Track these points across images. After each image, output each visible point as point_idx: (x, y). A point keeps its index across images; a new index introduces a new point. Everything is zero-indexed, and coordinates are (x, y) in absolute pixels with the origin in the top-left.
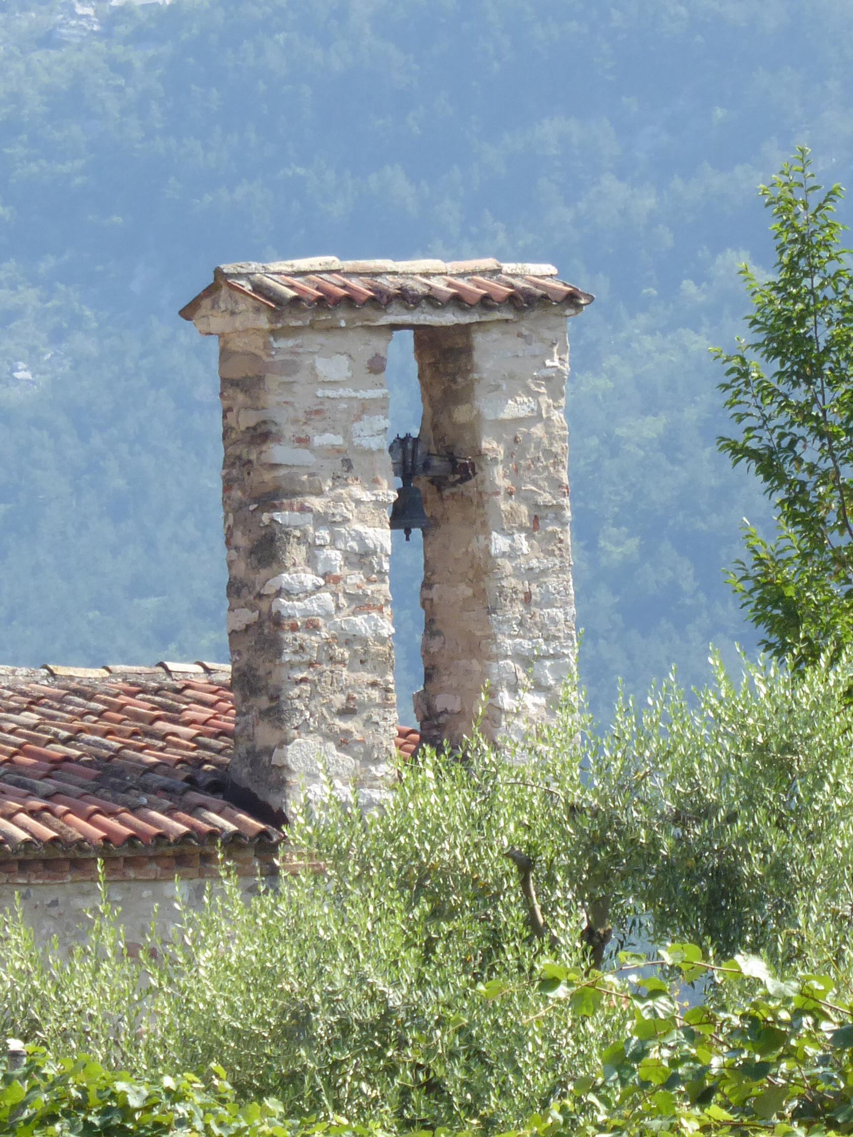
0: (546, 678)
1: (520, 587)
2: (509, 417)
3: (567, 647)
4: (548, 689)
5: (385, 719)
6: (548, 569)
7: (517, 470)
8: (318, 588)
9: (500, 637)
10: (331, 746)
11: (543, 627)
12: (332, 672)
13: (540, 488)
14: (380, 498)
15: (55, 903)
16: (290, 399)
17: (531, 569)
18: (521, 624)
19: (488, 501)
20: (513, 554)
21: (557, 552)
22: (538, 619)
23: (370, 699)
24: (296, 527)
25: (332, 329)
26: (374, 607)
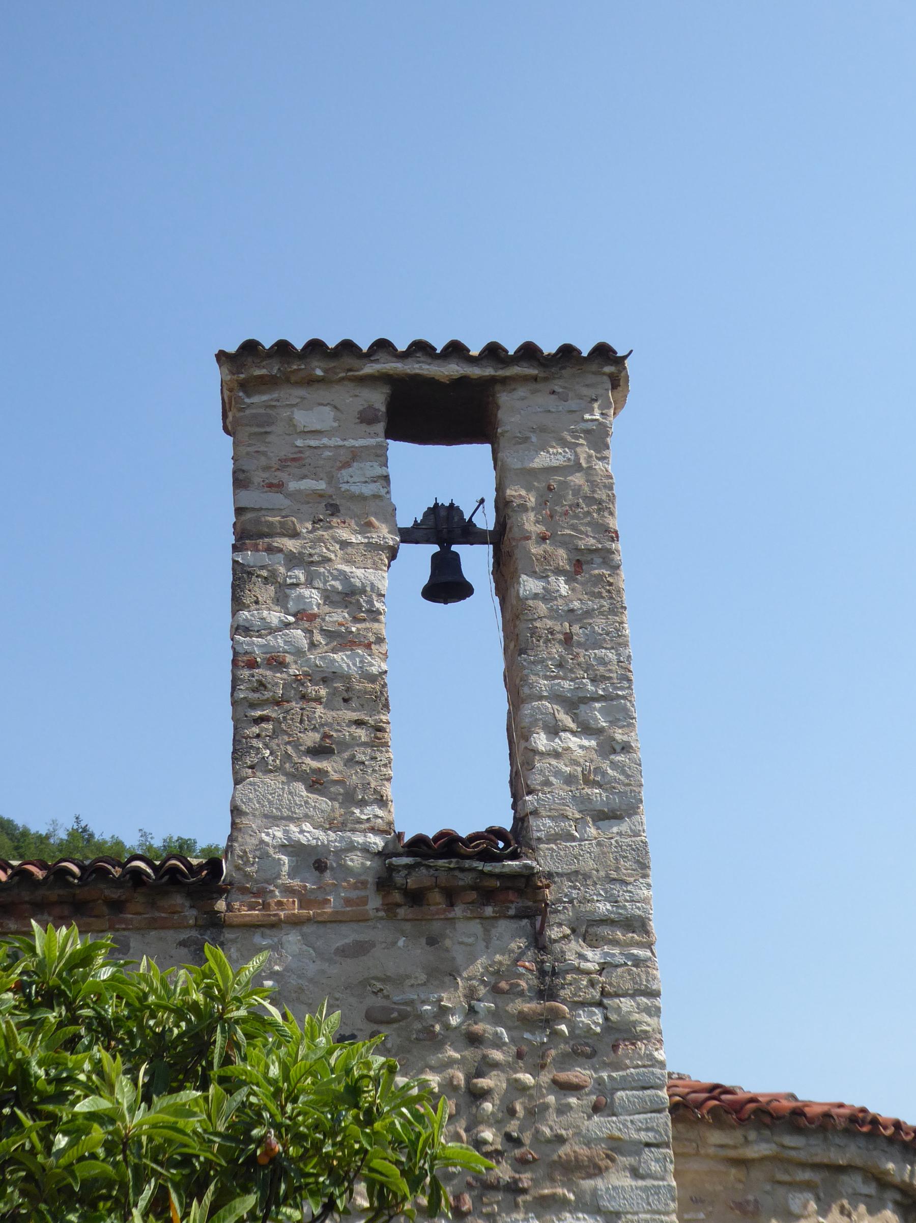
0: (596, 720)
1: (558, 628)
2: (540, 466)
3: (622, 689)
4: (599, 731)
5: (374, 758)
6: (593, 610)
7: (551, 516)
8: (288, 625)
9: (533, 678)
10: (300, 787)
11: (588, 668)
12: (302, 709)
13: (581, 532)
14: (374, 541)
16: (262, 449)
17: (572, 611)
18: (560, 666)
19: (517, 546)
20: (548, 596)
21: (605, 594)
22: (582, 659)
23: (353, 738)
24: (262, 567)
25: (311, 381)
26: (360, 644)
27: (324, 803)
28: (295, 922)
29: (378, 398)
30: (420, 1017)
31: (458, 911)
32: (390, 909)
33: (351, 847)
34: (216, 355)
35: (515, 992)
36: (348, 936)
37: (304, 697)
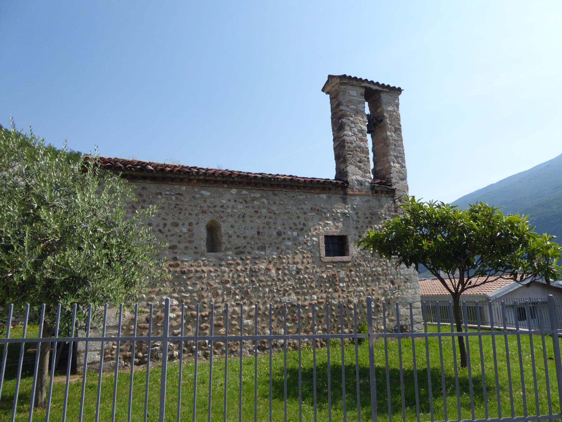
10: (357, 168)
15: (293, 197)
20: (392, 136)
25: (353, 85)
27: (361, 172)
28: (358, 195)
29: (363, 91)
30: (378, 214)
31: (383, 195)
32: (373, 193)
33: (366, 181)
34: (330, 77)
35: (391, 211)
36: (366, 198)
37: (356, 151)
